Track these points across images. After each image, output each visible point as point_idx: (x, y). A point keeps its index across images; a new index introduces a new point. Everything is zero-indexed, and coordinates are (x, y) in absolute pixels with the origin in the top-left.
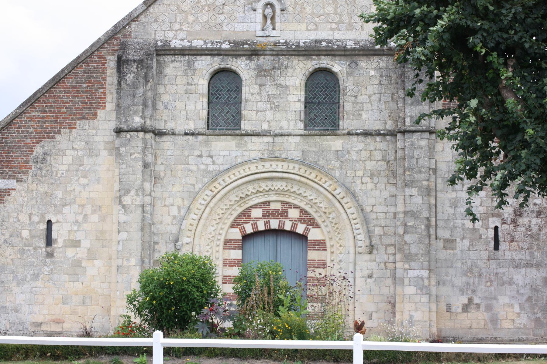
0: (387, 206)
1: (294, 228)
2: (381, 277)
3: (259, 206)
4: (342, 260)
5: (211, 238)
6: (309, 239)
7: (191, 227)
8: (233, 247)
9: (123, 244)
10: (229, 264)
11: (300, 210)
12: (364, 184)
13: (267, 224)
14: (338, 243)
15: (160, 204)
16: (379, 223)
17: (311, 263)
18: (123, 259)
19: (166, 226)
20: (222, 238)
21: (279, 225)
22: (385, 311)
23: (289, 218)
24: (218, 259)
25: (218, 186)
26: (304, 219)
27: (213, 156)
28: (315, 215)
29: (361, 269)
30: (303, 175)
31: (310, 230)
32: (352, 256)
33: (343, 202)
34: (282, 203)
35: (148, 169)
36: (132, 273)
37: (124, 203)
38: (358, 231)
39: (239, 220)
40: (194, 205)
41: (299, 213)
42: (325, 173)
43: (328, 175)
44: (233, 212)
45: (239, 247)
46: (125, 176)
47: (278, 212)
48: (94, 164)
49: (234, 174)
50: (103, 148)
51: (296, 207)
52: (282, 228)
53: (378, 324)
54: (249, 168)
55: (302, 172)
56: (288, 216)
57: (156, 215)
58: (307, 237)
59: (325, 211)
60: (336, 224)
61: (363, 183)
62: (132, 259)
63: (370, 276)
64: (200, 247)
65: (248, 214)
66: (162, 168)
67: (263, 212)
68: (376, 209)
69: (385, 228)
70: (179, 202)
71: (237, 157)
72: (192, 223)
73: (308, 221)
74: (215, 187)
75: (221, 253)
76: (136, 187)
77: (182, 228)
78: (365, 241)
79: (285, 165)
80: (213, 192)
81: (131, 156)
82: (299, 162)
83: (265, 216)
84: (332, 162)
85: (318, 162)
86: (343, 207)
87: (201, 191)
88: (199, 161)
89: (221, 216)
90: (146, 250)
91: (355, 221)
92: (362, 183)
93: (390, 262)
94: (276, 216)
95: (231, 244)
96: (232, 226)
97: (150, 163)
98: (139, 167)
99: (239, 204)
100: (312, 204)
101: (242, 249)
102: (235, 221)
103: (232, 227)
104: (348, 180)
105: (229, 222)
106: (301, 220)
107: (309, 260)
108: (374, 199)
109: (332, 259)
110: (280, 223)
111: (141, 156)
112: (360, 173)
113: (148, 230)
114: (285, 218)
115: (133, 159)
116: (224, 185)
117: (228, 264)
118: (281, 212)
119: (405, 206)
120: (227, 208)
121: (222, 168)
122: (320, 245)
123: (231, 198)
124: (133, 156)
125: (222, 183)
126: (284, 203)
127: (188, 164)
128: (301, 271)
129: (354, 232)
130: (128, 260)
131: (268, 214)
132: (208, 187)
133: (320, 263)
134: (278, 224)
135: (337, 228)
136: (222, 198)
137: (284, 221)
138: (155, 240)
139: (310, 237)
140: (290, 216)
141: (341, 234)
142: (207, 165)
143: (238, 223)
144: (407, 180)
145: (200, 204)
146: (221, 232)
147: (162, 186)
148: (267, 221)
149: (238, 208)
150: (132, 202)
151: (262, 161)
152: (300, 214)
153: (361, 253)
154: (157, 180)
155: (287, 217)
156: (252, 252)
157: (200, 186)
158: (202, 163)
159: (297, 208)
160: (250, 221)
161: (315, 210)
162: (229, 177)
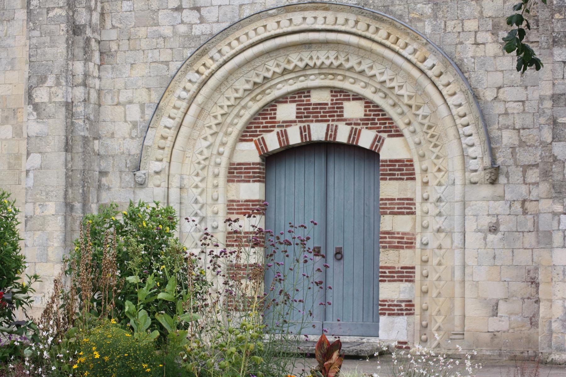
0: (526, 87)
1: (354, 138)
2: (515, 229)
3: (291, 98)
4: (443, 198)
5: (202, 162)
6: (381, 158)
7: (163, 141)
8: (245, 177)
9: (35, 176)
10: (238, 209)
11: (366, 103)
12: (480, 46)
13: (305, 131)
14: (435, 165)
15: (110, 102)
16: (510, 123)
17: (386, 204)
18: (34, 203)
19: (121, 141)
20: (224, 161)
21: (327, 134)
22: (523, 299)
23: (345, 120)
24: (217, 200)
25: (209, 62)
26: (374, 119)
27: (200, 7)
28: (392, 113)
29: (476, 215)
30: (364, 34)
31: (383, 141)
32: (458, 189)
33: (440, 82)
34: (332, 92)
35: (80, 37)
36: (49, 229)
37: (37, 100)
38: (469, 140)
39: (255, 127)
40: (167, 100)
41: (363, 109)
42: (403, 27)
43: (409, 31)
44: (242, 112)
45: (254, 177)
46: (39, 51)
47: (325, 108)
48: (6, 36)
49: (238, 39)
50: (19, 7)
51: (357, 97)
52: (332, 139)
53: (510, 324)
54: (265, 26)
55: (360, 29)
56: (342, 116)
57: (104, 121)
58: (378, 155)
59: (410, 102)
60: (430, 127)
61: (479, 44)
62: (50, 203)
63: (494, 229)
64: (182, 179)
65: (271, 114)
66: (113, 35)
67: (298, 109)
68: (505, 94)
69: (522, 131)
70: (142, 96)
71: (243, 7)
72: (165, 135)
73: (380, 124)
74: (204, 65)
75: (221, 189)
76: (56, 71)
77: (145, 143)
78: (482, 158)
79: (330, 16)
80: (202, 74)
81: (48, 13)
82: (355, 9)
83: (301, 117)
84: (419, 6)
85: (391, 8)
86: (441, 93)
87: (179, 73)
88: (175, 18)
89: (220, 119)
90: (78, 186)
91: (464, 120)
92: (477, 44)
93: (532, 201)
94: (321, 116)
95: (241, 173)
96: (243, 138)
97: (84, 26)
98: (62, 33)
99: (253, 95)
100: (387, 91)
101: (265, 182)
102: (248, 128)
103: (242, 141)
104: (449, 40)
105: (235, 131)
106: (367, 121)
107: (382, 199)
108: (500, 75)
109: (425, 196)
110: (328, 130)
111: (64, 14)
112: (471, 25)
113: (81, 150)
114: (338, 120)
115: (51, 20)
116: (221, 61)
117: (235, 209)
118: (330, 108)
119: (554, 84)
120: (229, 103)
121: (217, 28)
122: (403, 170)
123: (237, 85)
124: (51, 14)
125: (217, 56)
126: (336, 91)
127: (157, 25)
128: (372, 221)
129: (463, 142)
130: (43, 205)
131: (308, 113)
132: (191, 65)
133: (403, 204)
134: (325, 131)
135: (433, 136)
136: (221, 85)
137: (336, 126)
138: (102, 168)
139: (384, 155)
140: (346, 115)
141: (439, 148)
142: (191, 25)
143: (252, 132)
144: (556, 30)
145: (179, 98)
146: (221, 149)
147: (113, 68)
148: (304, 127)
149: (251, 103)
150: (50, 99)
151: (287, 12)
152: (366, 111)
153: (475, 183)
154: (106, 57)
155: (341, 118)
156: (283, 186)
157: (179, 64)
158: (182, 22)
159: (360, 99)
160: (274, 127)
161: (391, 102)
162: (229, 44)
